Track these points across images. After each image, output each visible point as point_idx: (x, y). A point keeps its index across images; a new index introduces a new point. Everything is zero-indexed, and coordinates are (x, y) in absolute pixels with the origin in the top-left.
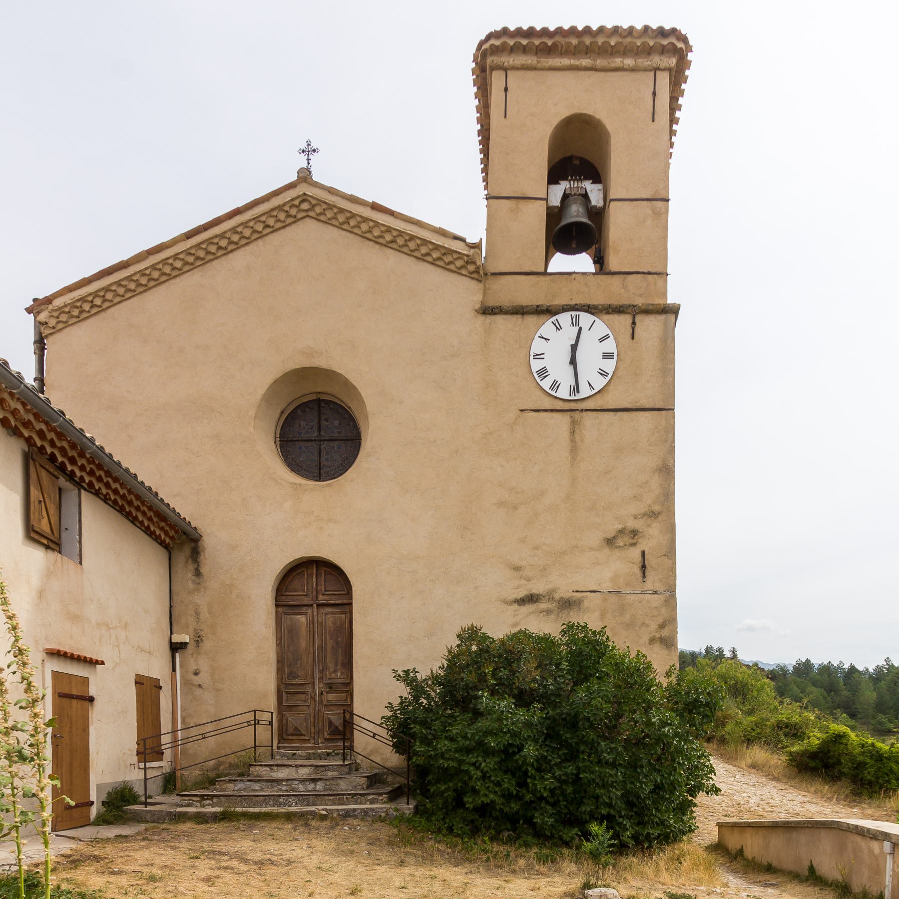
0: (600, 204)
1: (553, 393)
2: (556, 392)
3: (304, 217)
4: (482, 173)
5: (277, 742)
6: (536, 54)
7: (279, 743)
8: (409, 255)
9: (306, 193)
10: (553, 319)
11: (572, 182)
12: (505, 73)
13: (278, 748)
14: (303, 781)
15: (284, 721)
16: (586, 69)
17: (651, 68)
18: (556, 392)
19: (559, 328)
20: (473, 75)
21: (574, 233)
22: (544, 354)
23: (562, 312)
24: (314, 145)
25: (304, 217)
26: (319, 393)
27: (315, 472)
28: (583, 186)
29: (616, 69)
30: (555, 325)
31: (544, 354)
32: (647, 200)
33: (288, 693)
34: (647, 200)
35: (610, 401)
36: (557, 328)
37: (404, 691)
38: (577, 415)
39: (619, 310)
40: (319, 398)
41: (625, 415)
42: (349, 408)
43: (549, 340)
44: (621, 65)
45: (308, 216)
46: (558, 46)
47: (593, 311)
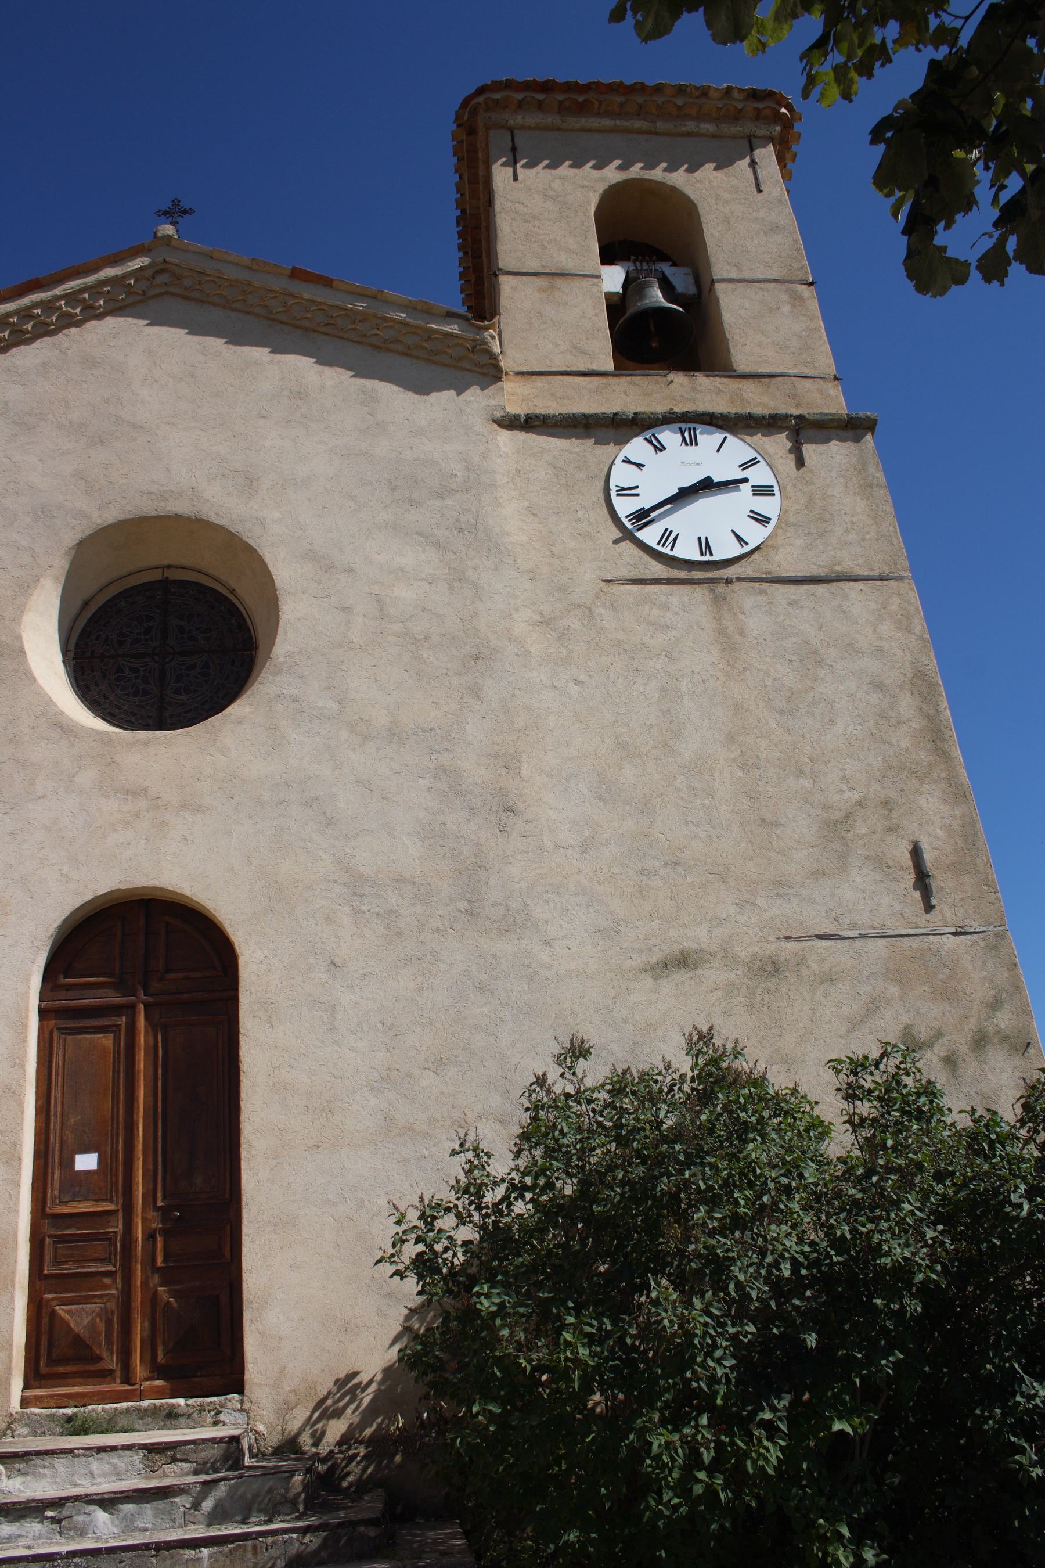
0: (692, 290)
1: (666, 550)
2: (672, 549)
3: (161, 294)
4: (461, 279)
5: (21, 1385)
6: (559, 112)
7: (25, 1388)
8: (359, 343)
9: (167, 259)
10: (648, 435)
11: (638, 264)
12: (509, 133)
13: (25, 1402)
14: (109, 1502)
15: (45, 1321)
16: (639, 132)
17: (742, 134)
18: (672, 549)
19: (660, 448)
20: (453, 141)
21: (652, 329)
22: (637, 487)
23: (662, 424)
24: (185, 204)
25: (161, 294)
26: (169, 567)
27: (150, 717)
28: (658, 268)
29: (689, 134)
30: (651, 442)
31: (637, 487)
32: (775, 281)
33: (58, 1239)
34: (775, 281)
35: (786, 562)
36: (656, 447)
37: (808, 449)
38: (721, 588)
39: (770, 424)
40: (167, 578)
41: (820, 589)
42: (233, 591)
43: (643, 466)
44: (696, 130)
45: (167, 293)
46: (593, 103)
47: (720, 422)
